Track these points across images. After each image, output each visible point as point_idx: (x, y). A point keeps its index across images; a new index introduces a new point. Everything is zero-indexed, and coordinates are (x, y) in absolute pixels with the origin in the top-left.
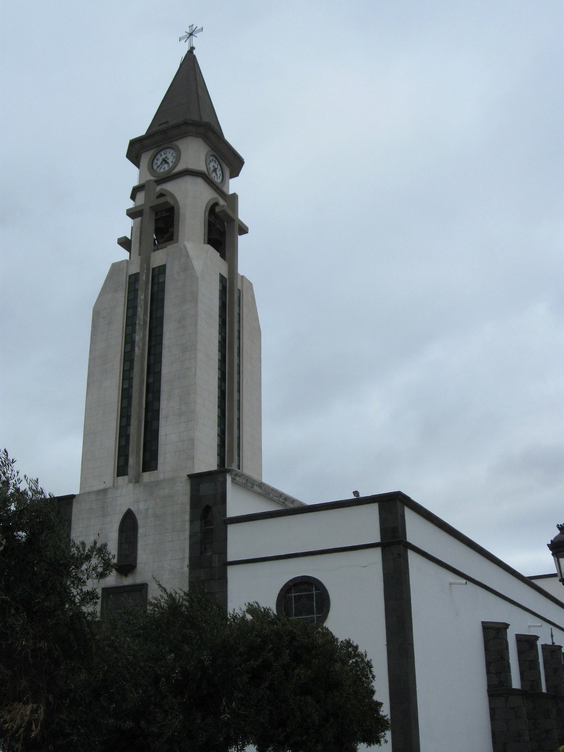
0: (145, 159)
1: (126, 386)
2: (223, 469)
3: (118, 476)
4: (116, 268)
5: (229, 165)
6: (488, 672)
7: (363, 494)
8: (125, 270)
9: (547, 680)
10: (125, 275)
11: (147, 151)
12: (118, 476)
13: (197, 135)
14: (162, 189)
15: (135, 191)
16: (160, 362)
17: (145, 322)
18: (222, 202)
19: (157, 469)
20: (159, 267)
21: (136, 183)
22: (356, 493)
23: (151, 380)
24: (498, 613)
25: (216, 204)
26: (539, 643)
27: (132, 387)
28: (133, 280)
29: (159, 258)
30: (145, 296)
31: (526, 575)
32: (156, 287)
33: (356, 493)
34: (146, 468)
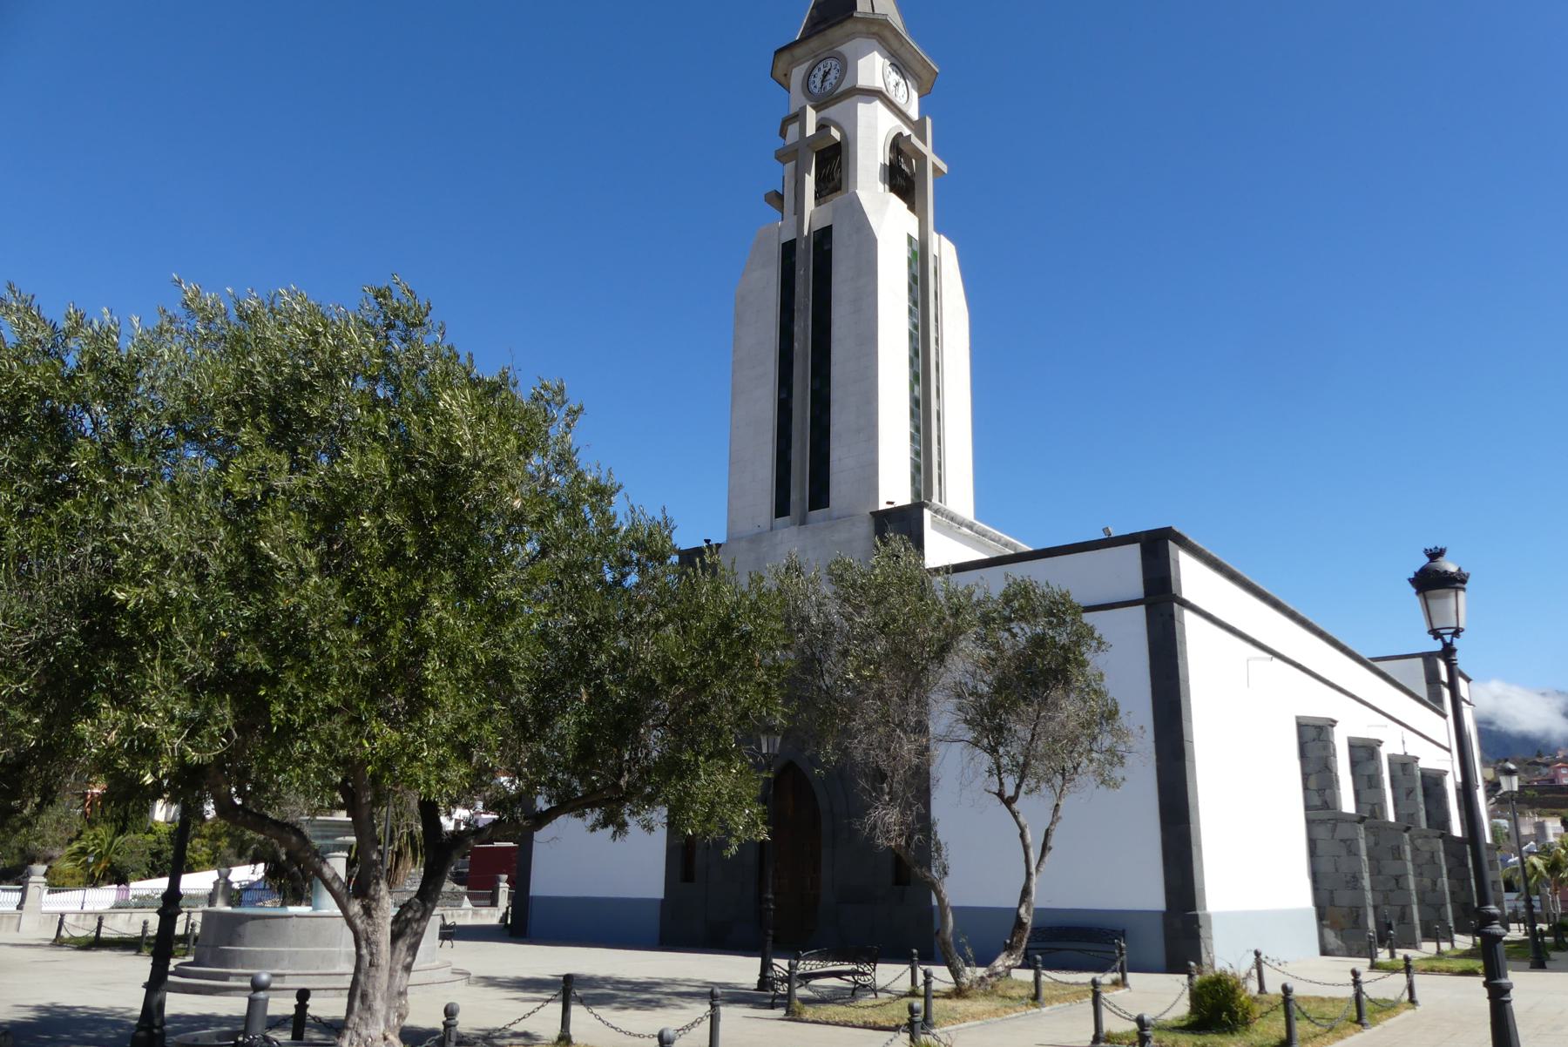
6: (1306, 788)
7: (1115, 532)
9: (1396, 805)
22: (1106, 530)
24: (1320, 704)
25: (900, 134)
26: (1384, 752)
28: (789, 249)
31: (1365, 656)
33: (1106, 530)
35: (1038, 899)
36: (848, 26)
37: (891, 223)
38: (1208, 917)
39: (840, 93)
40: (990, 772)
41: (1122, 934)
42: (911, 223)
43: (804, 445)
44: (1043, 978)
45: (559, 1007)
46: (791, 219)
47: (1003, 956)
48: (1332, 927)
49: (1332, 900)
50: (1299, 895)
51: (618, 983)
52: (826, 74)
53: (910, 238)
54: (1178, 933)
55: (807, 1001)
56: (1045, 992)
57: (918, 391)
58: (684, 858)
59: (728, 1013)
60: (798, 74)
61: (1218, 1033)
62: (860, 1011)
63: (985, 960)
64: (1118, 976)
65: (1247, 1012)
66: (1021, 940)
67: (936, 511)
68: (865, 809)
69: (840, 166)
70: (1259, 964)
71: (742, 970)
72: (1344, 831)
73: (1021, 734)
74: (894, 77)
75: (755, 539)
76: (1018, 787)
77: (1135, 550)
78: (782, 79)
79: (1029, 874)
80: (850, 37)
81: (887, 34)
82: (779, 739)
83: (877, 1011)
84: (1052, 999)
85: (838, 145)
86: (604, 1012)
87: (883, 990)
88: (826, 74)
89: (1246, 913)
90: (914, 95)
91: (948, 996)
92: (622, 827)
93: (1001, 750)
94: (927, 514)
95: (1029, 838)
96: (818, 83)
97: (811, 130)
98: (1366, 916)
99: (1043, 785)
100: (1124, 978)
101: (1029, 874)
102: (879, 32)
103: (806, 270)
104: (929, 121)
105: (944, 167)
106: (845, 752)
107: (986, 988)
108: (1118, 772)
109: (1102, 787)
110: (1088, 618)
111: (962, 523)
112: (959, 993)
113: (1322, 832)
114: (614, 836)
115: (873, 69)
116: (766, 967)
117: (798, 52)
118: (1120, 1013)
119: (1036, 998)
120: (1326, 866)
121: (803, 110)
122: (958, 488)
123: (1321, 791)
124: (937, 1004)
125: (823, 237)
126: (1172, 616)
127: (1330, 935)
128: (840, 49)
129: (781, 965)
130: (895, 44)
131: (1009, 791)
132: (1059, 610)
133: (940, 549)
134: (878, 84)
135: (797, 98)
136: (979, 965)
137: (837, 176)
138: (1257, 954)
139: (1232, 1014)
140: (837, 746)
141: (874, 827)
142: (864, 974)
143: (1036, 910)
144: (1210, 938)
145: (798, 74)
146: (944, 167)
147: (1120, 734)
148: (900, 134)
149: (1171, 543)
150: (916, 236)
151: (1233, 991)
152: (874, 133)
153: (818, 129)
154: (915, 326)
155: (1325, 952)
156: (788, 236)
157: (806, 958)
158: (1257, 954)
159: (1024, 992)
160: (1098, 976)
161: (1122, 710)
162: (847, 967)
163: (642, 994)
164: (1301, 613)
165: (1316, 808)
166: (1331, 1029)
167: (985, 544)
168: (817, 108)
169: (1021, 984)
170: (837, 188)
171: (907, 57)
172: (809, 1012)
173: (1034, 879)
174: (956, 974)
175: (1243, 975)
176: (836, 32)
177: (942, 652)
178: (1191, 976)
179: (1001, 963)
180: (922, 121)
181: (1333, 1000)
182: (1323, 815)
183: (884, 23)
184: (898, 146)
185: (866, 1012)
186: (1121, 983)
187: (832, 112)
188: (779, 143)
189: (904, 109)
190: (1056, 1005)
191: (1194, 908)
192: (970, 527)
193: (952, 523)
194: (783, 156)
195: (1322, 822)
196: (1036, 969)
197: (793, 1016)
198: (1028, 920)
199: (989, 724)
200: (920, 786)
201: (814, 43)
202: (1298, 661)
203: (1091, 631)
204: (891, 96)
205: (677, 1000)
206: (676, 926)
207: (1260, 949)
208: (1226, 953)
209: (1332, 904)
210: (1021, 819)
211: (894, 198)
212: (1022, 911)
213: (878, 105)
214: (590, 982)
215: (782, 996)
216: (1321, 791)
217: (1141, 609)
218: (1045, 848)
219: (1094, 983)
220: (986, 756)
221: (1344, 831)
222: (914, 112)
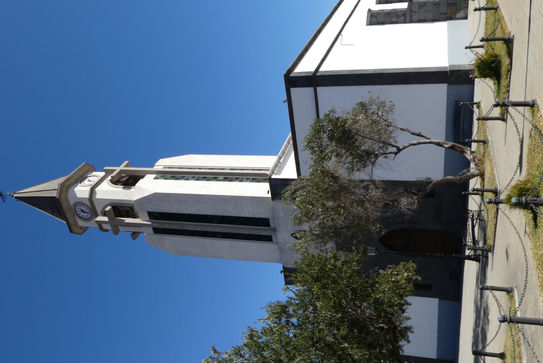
1: (220, 236)
6: (397, 23)
7: (285, 98)
22: (284, 102)
24: (361, 15)
25: (111, 180)
28: (157, 231)
33: (284, 102)
35: (441, 140)
36: (62, 200)
37: (148, 186)
38: (450, 66)
39: (91, 205)
40: (386, 157)
41: (457, 103)
42: (149, 178)
43: (242, 228)
44: (476, 139)
45: (487, 358)
46: (144, 229)
47: (466, 155)
48: (455, 15)
49: (444, 14)
50: (442, 27)
51: (477, 324)
52: (82, 211)
53: (155, 178)
54: (455, 79)
55: (485, 242)
56: (482, 138)
57: (221, 177)
58: (421, 289)
59: (489, 283)
60: (81, 223)
61: (501, 69)
62: (490, 219)
63: (467, 164)
64: (475, 106)
65: (492, 56)
66: (459, 147)
67: (273, 172)
68: (402, 215)
69: (122, 207)
70: (470, 48)
71: (471, 269)
72: (415, 8)
73: (370, 144)
74: (86, 182)
75: (282, 251)
76: (393, 146)
77: (293, 90)
78: (83, 230)
79: (431, 143)
80: (67, 200)
81: (67, 184)
82: (369, 248)
83: (489, 212)
84: (485, 136)
85: (113, 207)
86: (489, 337)
87: (480, 208)
88: (82, 211)
89: (449, 52)
90: (94, 173)
91: (483, 180)
92: (408, 329)
93: (376, 152)
94: (274, 177)
95: (415, 142)
96: (86, 215)
97: (106, 219)
98: (448, 179)
99: (392, 135)
100: (476, 103)
101: (431, 143)
102: (66, 187)
103: (167, 223)
104: (106, 168)
105: (126, 162)
106: (376, 220)
107: (480, 163)
108: (388, 104)
109: (394, 111)
110: (322, 116)
111: (278, 162)
112: (482, 175)
113: (415, 17)
114: (412, 332)
115: (82, 191)
116: (469, 258)
117: (72, 222)
118: (491, 110)
119: (484, 142)
120: (430, 16)
121: (97, 222)
122: (264, 162)
123: (398, 16)
124: (487, 187)
125: (152, 215)
126: (322, 76)
127: (458, 15)
128: (72, 205)
129: (467, 252)
130: (72, 181)
131: (394, 150)
132: (318, 130)
133: (289, 171)
134: (88, 189)
135: (91, 224)
136: (469, 166)
137: (127, 208)
138: (467, 48)
139: (493, 62)
140: (374, 224)
141: (409, 209)
142: (473, 215)
143: (446, 140)
144: (459, 65)
145: (81, 223)
146: (126, 162)
147: (372, 102)
148: (111, 180)
149: (291, 75)
150: (155, 176)
151: (482, 61)
152: (109, 192)
153: (106, 216)
154: (193, 178)
155: (466, 18)
156: (151, 231)
157: (466, 241)
158: (467, 48)
159: (482, 147)
160: (475, 117)
161: (360, 100)
162: (470, 223)
163: (482, 314)
164: (323, 21)
165: (405, 19)
166: (499, 21)
167: (288, 152)
168: (97, 216)
169: (478, 147)
170: (132, 208)
171: (77, 176)
172: (490, 242)
173: (433, 140)
174: (473, 176)
175: (476, 57)
176: (65, 206)
177: (335, 179)
178: (476, 77)
179: (469, 156)
180: (106, 171)
181: (486, 18)
182: (408, 16)
183: (62, 185)
184: (115, 182)
185: (490, 217)
186: (478, 105)
187: (99, 209)
188: (111, 233)
189: (100, 178)
190: (488, 133)
191: (447, 72)
192: (280, 158)
193: (278, 166)
194: (116, 231)
195: (411, 16)
196: (472, 142)
197: (491, 249)
198: (450, 144)
199: (366, 158)
200: (391, 186)
201: (68, 215)
202: (343, 23)
203: (327, 116)
204: (94, 183)
205: (484, 300)
206: (451, 294)
207: (465, 47)
208: (467, 60)
209: (446, 14)
210: (407, 145)
211: (138, 184)
212: (446, 146)
213: (97, 189)
214: (475, 343)
215: (483, 253)
216: (398, 16)
217: (319, 89)
218: (419, 135)
219: (478, 119)
220: (379, 159)
221: (415, 8)
222: (102, 174)
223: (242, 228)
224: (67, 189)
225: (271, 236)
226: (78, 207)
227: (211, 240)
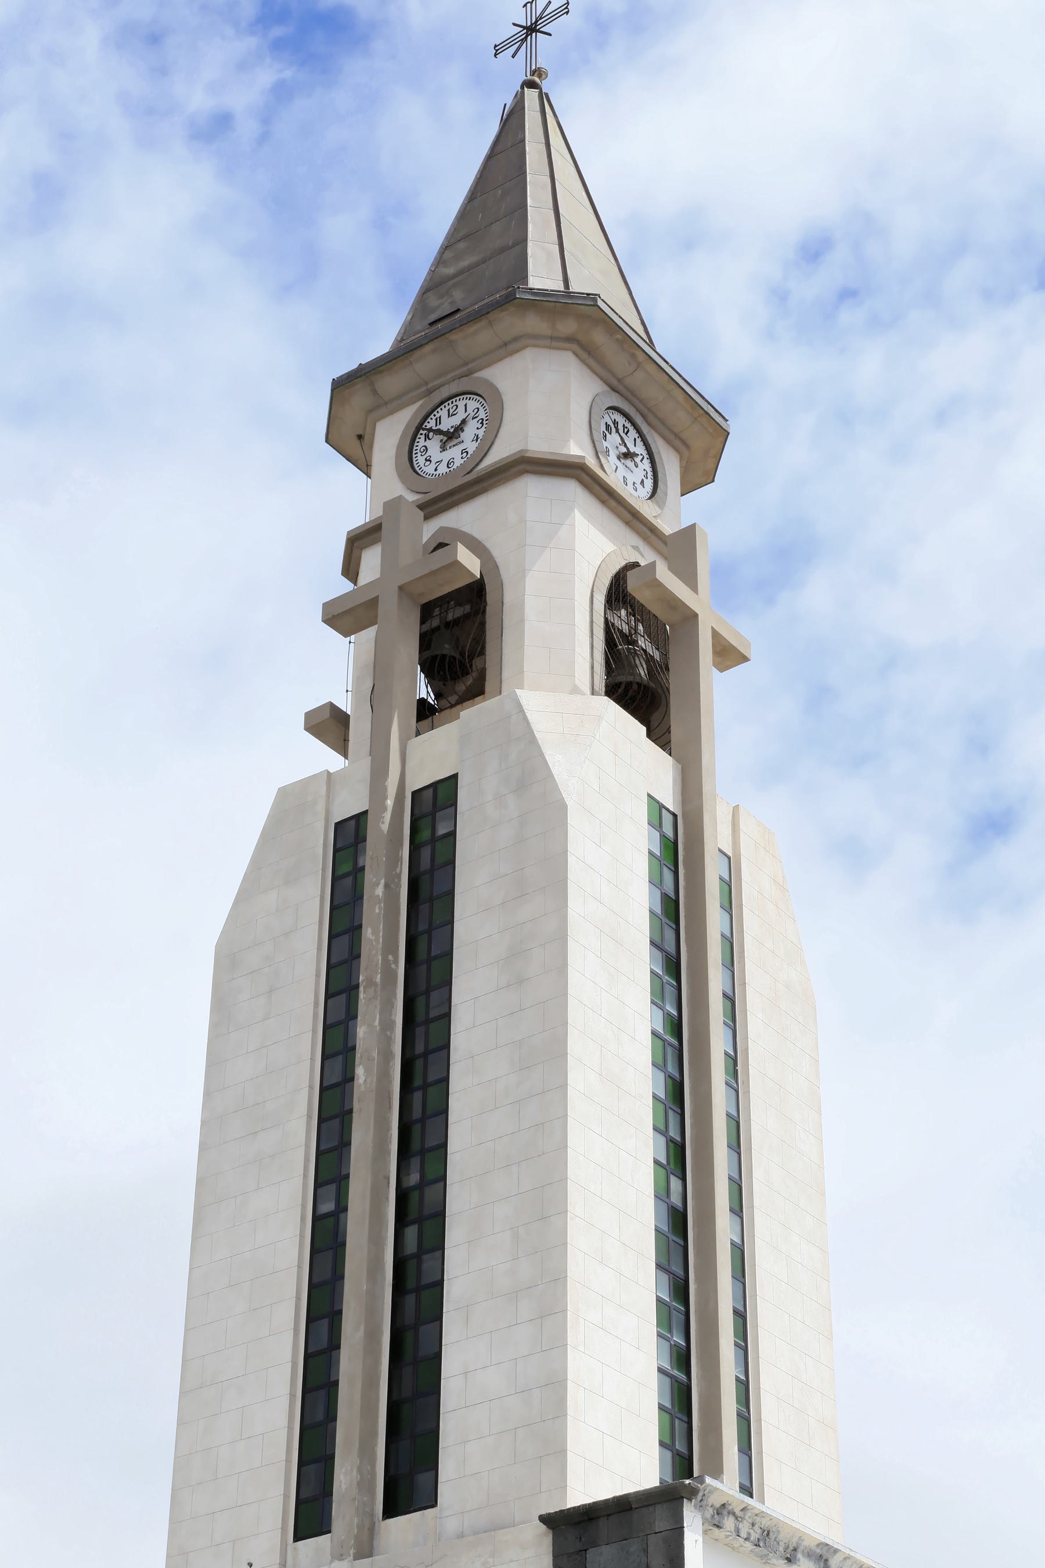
0: (388, 436)
2: (669, 1498)
3: (297, 1538)
4: (290, 803)
5: (678, 442)
8: (321, 807)
10: (320, 825)
11: (392, 413)
12: (297, 1538)
13: (556, 342)
14: (443, 530)
15: (358, 541)
16: (444, 1111)
17: (389, 976)
18: (645, 556)
19: (434, 1504)
20: (435, 785)
21: (359, 517)
23: (414, 1178)
27: (345, 1209)
28: (350, 836)
29: (433, 754)
30: (387, 886)
32: (426, 853)
34: (396, 1503)
42: (654, 771)
53: (657, 808)
80: (508, 347)
81: (599, 337)
103: (391, 888)
117: (390, 384)
150: (669, 799)
162: (380, 946)
170: (477, 692)
201: (426, 363)
223: (376, 1241)
224: (570, 339)
225: (329, 1532)
226: (472, 405)
227: (301, 1153)
